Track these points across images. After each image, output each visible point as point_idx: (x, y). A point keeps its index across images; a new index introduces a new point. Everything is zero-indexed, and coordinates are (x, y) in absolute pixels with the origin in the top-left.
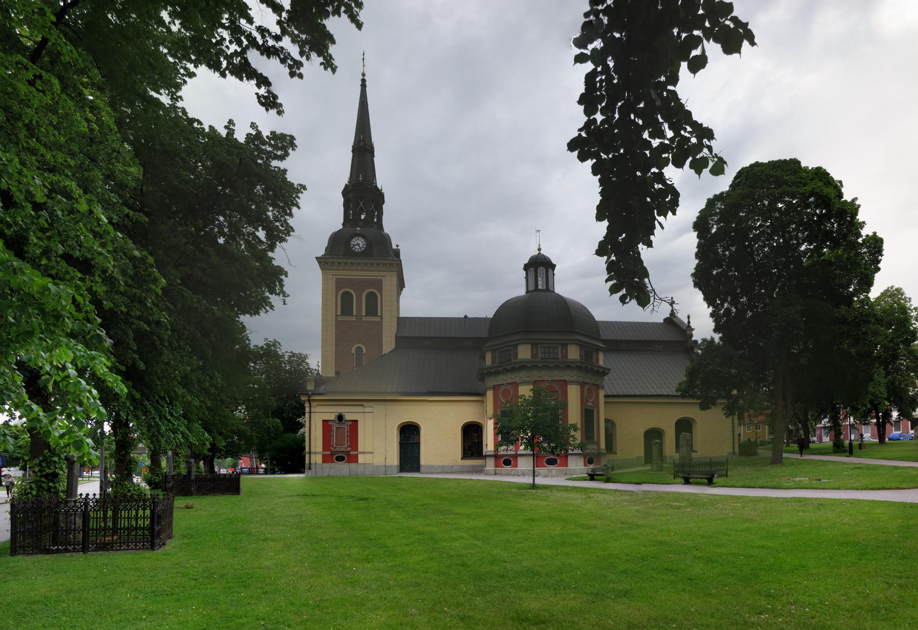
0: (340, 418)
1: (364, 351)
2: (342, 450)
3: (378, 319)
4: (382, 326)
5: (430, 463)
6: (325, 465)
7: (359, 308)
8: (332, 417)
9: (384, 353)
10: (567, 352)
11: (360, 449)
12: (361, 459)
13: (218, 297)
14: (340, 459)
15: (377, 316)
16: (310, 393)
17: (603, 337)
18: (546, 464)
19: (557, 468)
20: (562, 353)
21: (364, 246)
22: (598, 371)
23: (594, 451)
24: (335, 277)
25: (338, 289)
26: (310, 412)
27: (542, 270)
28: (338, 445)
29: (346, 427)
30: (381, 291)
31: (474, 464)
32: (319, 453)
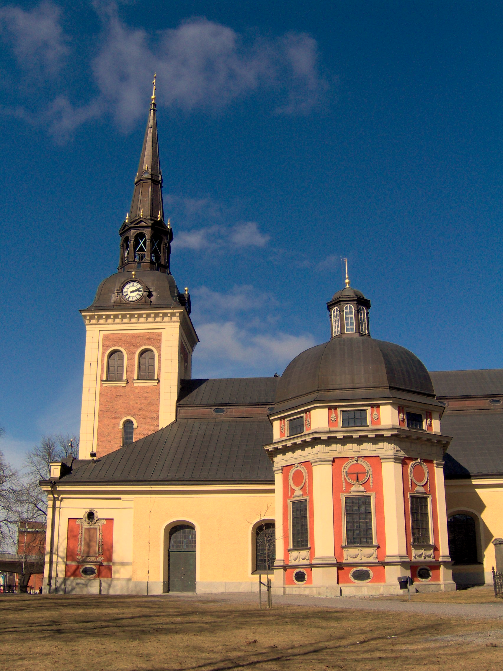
0: (91, 515)
3: (153, 383)
10: (379, 415)
13: (186, 287)
15: (154, 379)
18: (352, 579)
19: (370, 584)
20: (372, 418)
21: (127, 297)
22: (429, 440)
23: (428, 559)
24: (102, 333)
25: (105, 348)
30: (159, 348)
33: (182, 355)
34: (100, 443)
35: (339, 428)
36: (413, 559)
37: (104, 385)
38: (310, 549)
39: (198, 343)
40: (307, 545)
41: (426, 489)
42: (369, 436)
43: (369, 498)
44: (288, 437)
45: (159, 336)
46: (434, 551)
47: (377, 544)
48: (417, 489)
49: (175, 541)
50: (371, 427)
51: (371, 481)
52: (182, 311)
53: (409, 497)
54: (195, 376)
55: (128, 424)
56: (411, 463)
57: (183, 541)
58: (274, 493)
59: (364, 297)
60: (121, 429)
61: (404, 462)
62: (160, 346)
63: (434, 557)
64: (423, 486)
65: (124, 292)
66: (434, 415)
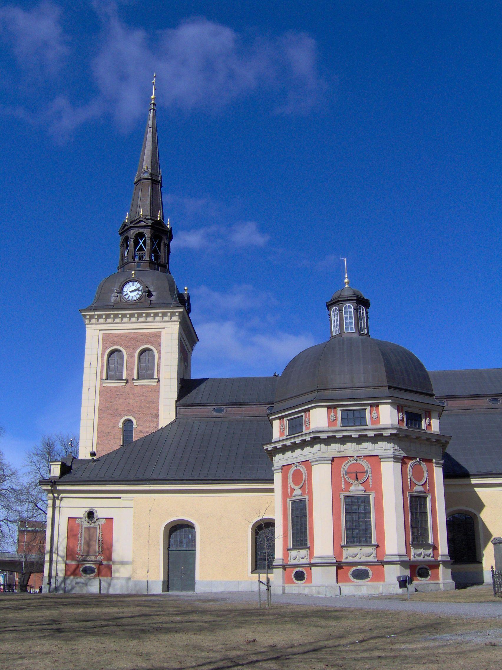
0: (91, 515)
3: (153, 383)
10: (378, 415)
15: (154, 379)
18: (352, 578)
20: (371, 418)
22: (428, 439)
23: (427, 558)
24: (102, 332)
25: (105, 347)
30: (159, 347)
33: (182, 355)
35: (339, 428)
36: (412, 559)
37: (104, 385)
39: (198, 343)
40: (306, 544)
41: (425, 489)
44: (287, 436)
46: (433, 550)
47: (376, 544)
48: (417, 488)
50: (370, 426)
51: (371, 481)
52: (182, 310)
53: (408, 496)
54: (195, 375)
56: (410, 463)
61: (403, 461)
63: (433, 557)
64: (422, 485)
66: (433, 414)
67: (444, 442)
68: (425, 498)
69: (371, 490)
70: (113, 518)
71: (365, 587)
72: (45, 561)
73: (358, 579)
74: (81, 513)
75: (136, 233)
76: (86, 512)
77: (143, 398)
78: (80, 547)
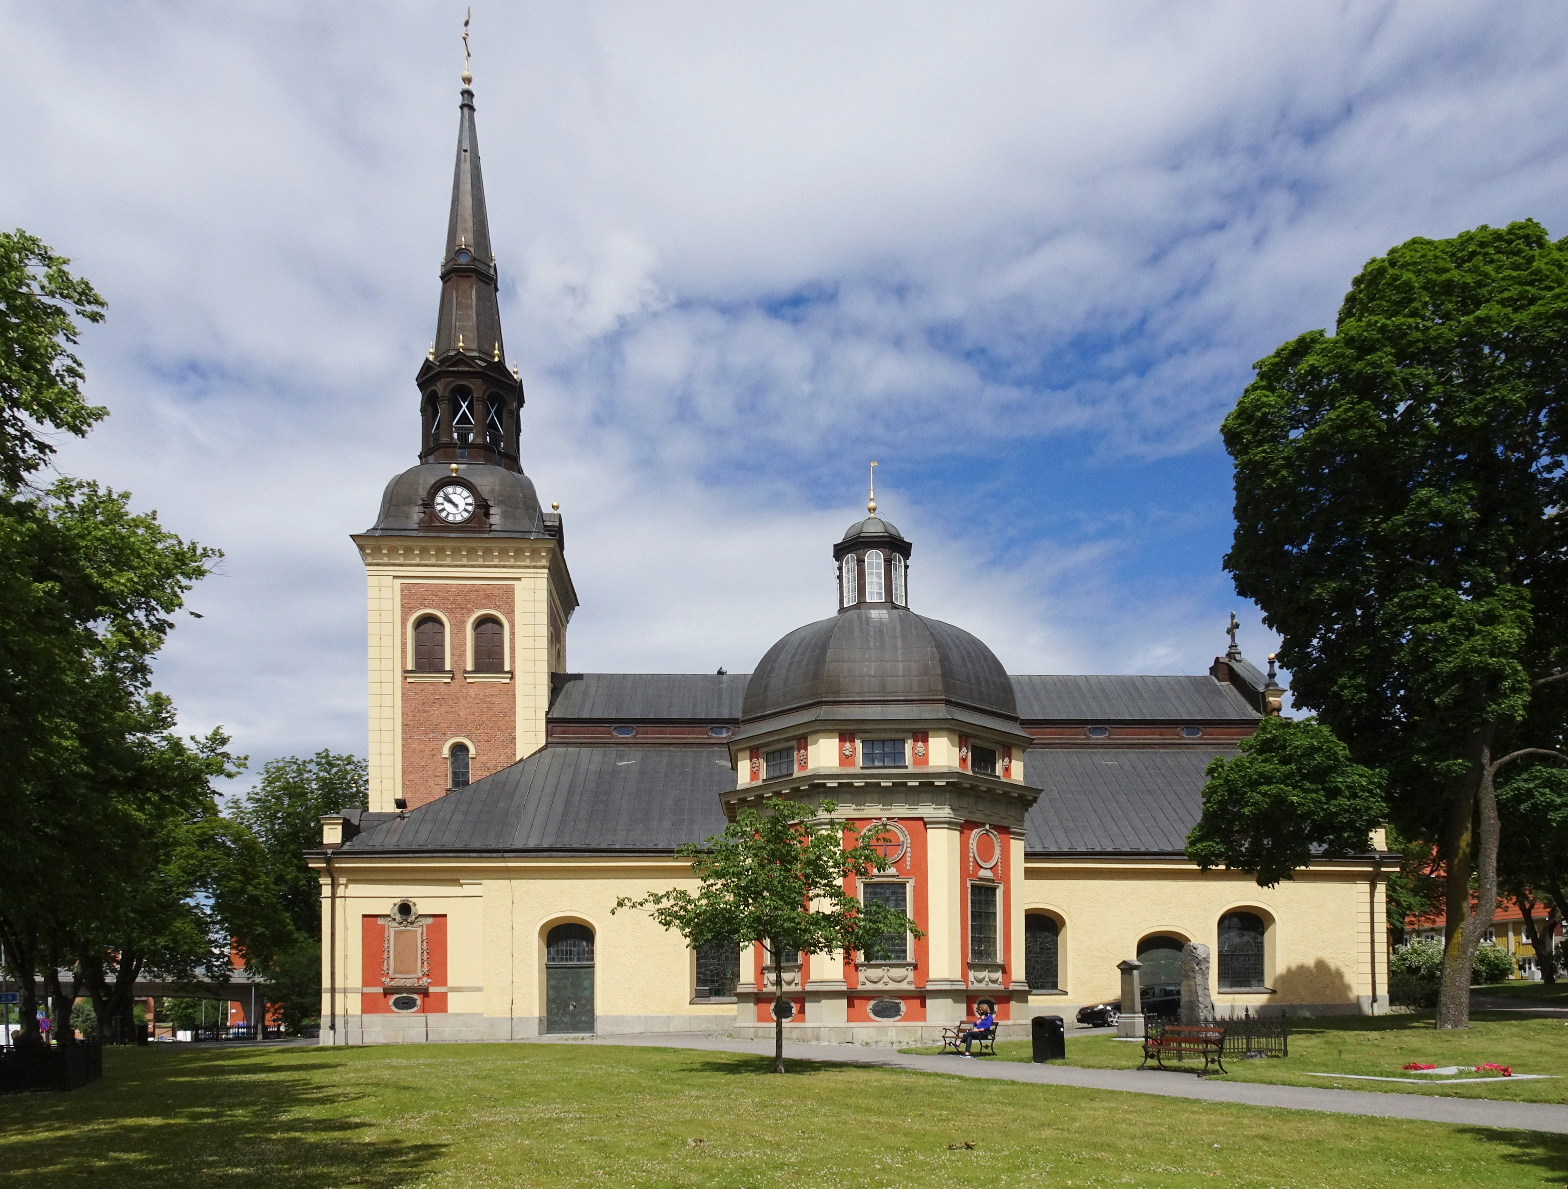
0: (405, 909)
1: (472, 752)
2: (409, 983)
4: (514, 695)
5: (617, 1012)
6: (367, 1017)
7: (458, 653)
8: (386, 907)
9: (518, 759)
10: (927, 750)
11: (451, 982)
12: (455, 1003)
14: (405, 1004)
16: (330, 851)
17: (1023, 713)
18: (393, 1008)
20: (915, 754)
21: (470, 508)
22: (1006, 794)
23: (993, 986)
25: (406, 610)
26: (333, 897)
27: (874, 559)
28: (399, 973)
29: (419, 931)
30: (510, 613)
31: (720, 1013)
32: (354, 991)
33: (551, 629)
34: (407, 783)
35: (857, 770)
36: (971, 987)
37: (409, 680)
38: (800, 967)
39: (577, 608)
40: (796, 960)
41: (995, 874)
42: (828, 785)
43: (903, 885)
44: (764, 780)
45: (509, 593)
46: (1003, 972)
47: (914, 961)
48: (983, 873)
49: (558, 951)
50: (911, 770)
51: (908, 859)
52: (552, 546)
53: (969, 886)
54: (571, 668)
55: (459, 750)
56: (975, 833)
57: (571, 950)
58: (1026, 878)
59: (902, 536)
60: (446, 758)
61: (965, 827)
62: (513, 611)
63: (1004, 983)
64: (991, 869)
65: (438, 504)
66: (1015, 752)
67: (1031, 798)
68: (994, 889)
69: (909, 874)
70: (445, 916)
71: (894, 1030)
72: (323, 990)
73: (883, 1017)
74: (386, 907)
75: (454, 385)
76: (395, 905)
77: (485, 706)
78: (388, 964)
